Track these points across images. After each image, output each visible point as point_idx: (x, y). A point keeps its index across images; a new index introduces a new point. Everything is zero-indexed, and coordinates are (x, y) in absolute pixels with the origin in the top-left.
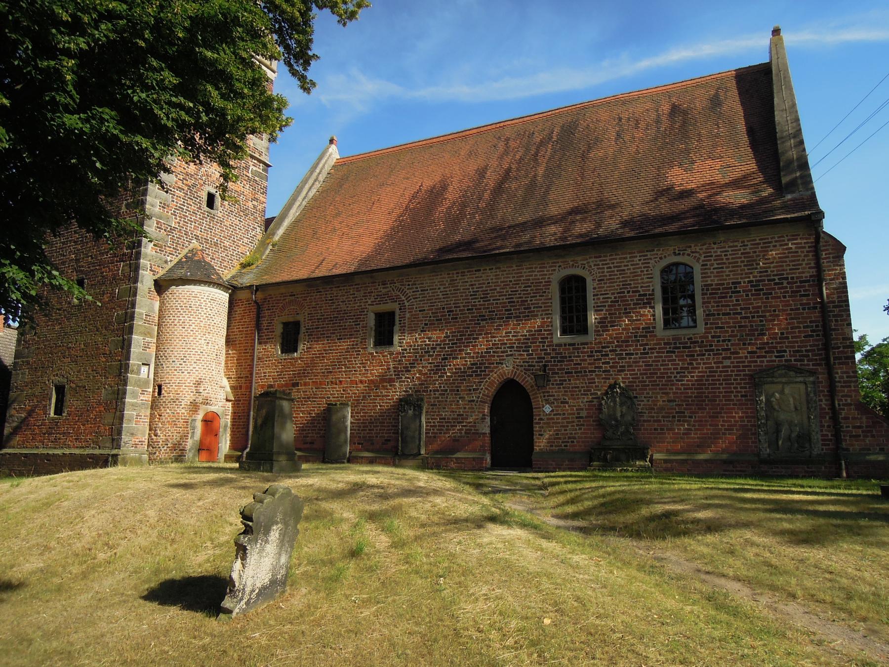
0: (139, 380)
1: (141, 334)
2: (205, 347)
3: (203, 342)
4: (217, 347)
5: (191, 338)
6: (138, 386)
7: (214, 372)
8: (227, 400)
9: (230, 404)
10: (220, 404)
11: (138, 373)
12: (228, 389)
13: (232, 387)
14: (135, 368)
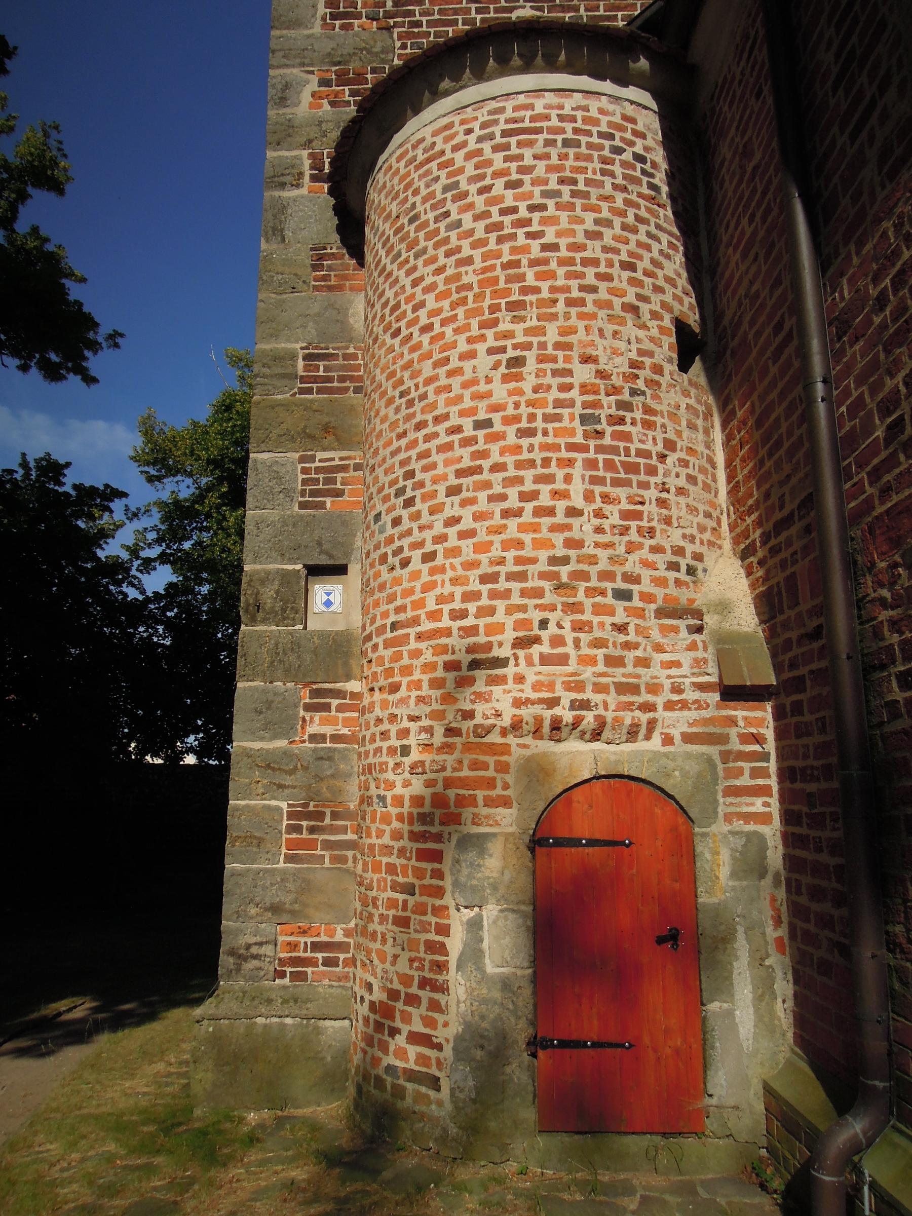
0: (296, 645)
1: (288, 439)
2: (500, 392)
3: (484, 362)
4: (583, 374)
5: (427, 369)
6: (289, 674)
7: (583, 528)
8: (732, 693)
9: (761, 718)
10: (678, 723)
11: (294, 606)
12: (746, 619)
13: (769, 605)
14: (268, 594)
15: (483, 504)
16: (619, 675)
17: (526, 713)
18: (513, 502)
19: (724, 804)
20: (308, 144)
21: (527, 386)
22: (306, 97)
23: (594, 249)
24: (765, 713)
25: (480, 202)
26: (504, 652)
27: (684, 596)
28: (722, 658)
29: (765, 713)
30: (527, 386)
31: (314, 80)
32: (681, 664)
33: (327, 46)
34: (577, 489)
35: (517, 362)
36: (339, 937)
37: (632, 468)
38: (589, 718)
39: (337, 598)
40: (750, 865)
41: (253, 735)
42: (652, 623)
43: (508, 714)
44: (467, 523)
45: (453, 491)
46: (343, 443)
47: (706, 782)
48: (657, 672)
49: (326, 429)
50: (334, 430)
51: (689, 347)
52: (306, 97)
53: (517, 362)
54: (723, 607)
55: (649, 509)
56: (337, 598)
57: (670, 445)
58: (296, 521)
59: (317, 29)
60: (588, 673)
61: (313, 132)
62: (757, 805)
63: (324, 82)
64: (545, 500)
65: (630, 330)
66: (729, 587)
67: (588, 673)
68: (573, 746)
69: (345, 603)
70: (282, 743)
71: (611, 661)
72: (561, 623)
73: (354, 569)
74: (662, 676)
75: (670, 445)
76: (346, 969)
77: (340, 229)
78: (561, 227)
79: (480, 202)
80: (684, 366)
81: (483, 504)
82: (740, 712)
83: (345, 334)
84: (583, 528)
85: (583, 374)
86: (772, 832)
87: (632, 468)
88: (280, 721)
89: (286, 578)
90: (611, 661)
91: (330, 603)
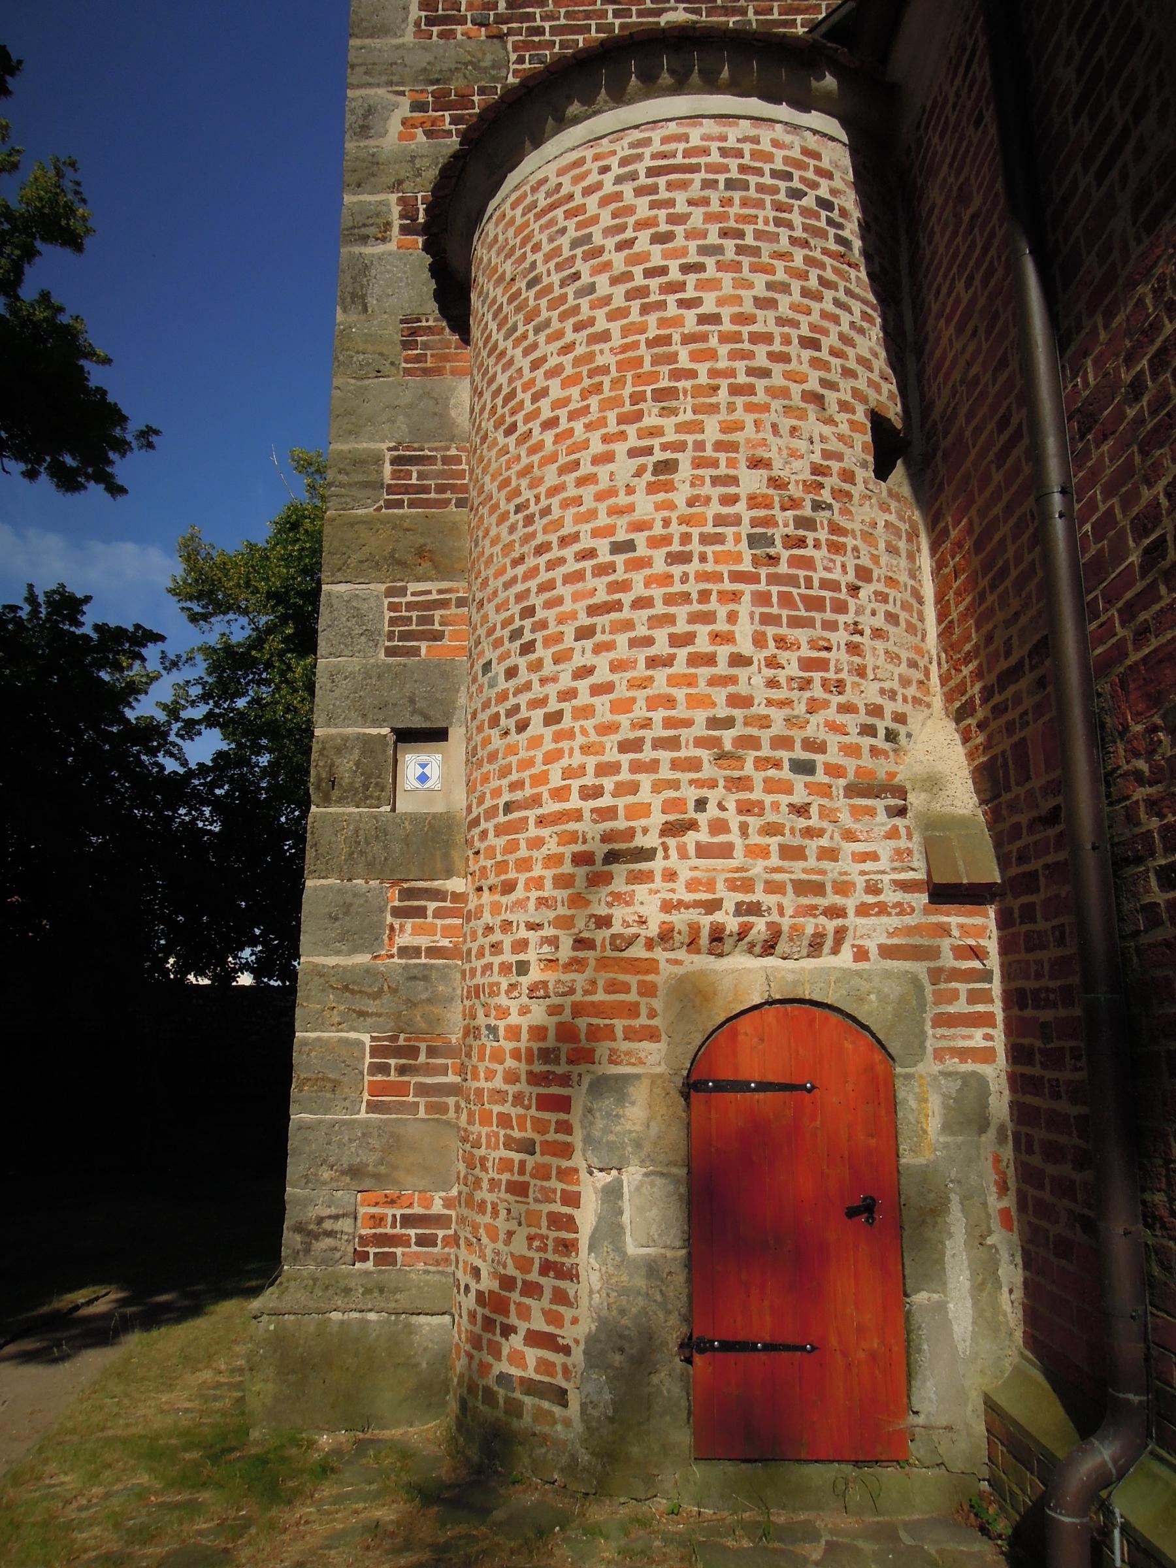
0: (381, 832)
1: (372, 567)
2: (644, 505)
3: (624, 466)
4: (752, 482)
5: (551, 476)
6: (373, 869)
7: (752, 681)
8: (943, 894)
9: (982, 926)
10: (874, 932)
11: (379, 782)
12: (961, 798)
13: (992, 780)
14: (346, 766)
15: (622, 650)
16: (798, 870)
17: (678, 919)
18: (661, 647)
19: (934, 1037)
20: (397, 185)
21: (680, 497)
22: (394, 126)
23: (765, 322)
24: (987, 919)
25: (619, 260)
26: (651, 841)
27: (882, 768)
28: (931, 848)
29: (987, 919)
30: (680, 497)
31: (405, 103)
32: (878, 857)
33: (422, 59)
34: (744, 631)
35: (667, 467)
36: (437, 1208)
37: (815, 604)
38: (760, 926)
39: (434, 771)
40: (968, 1115)
41: (327, 948)
42: (841, 803)
43: (655, 921)
44: (602, 674)
45: (584, 633)
46: (442, 572)
47: (910, 1008)
48: (847, 867)
49: (421, 553)
50: (431, 555)
51: (888, 447)
52: (394, 126)
53: (667, 467)
54: (933, 783)
55: (837, 656)
56: (434, 771)
57: (864, 574)
58: (382, 672)
59: (409, 38)
60: (758, 868)
61: (404, 171)
62: (977, 1038)
63: (418, 106)
64: (702, 645)
65: (812, 425)
66: (940, 756)
67: (758, 868)
68: (739, 962)
69: (445, 778)
70: (363, 959)
71: (788, 853)
72: (723, 803)
73: (457, 733)
74: (854, 871)
75: (864, 574)
76: (447, 1250)
77: (439, 296)
78: (724, 292)
79: (619, 260)
80: (882, 472)
81: (622, 650)
82: (955, 919)
83: (445, 430)
84: (752, 681)
85: (752, 482)
86: (995, 1073)
87: (815, 604)
88: (361, 930)
89: (369, 745)
90: (788, 853)
91: (425, 777)
